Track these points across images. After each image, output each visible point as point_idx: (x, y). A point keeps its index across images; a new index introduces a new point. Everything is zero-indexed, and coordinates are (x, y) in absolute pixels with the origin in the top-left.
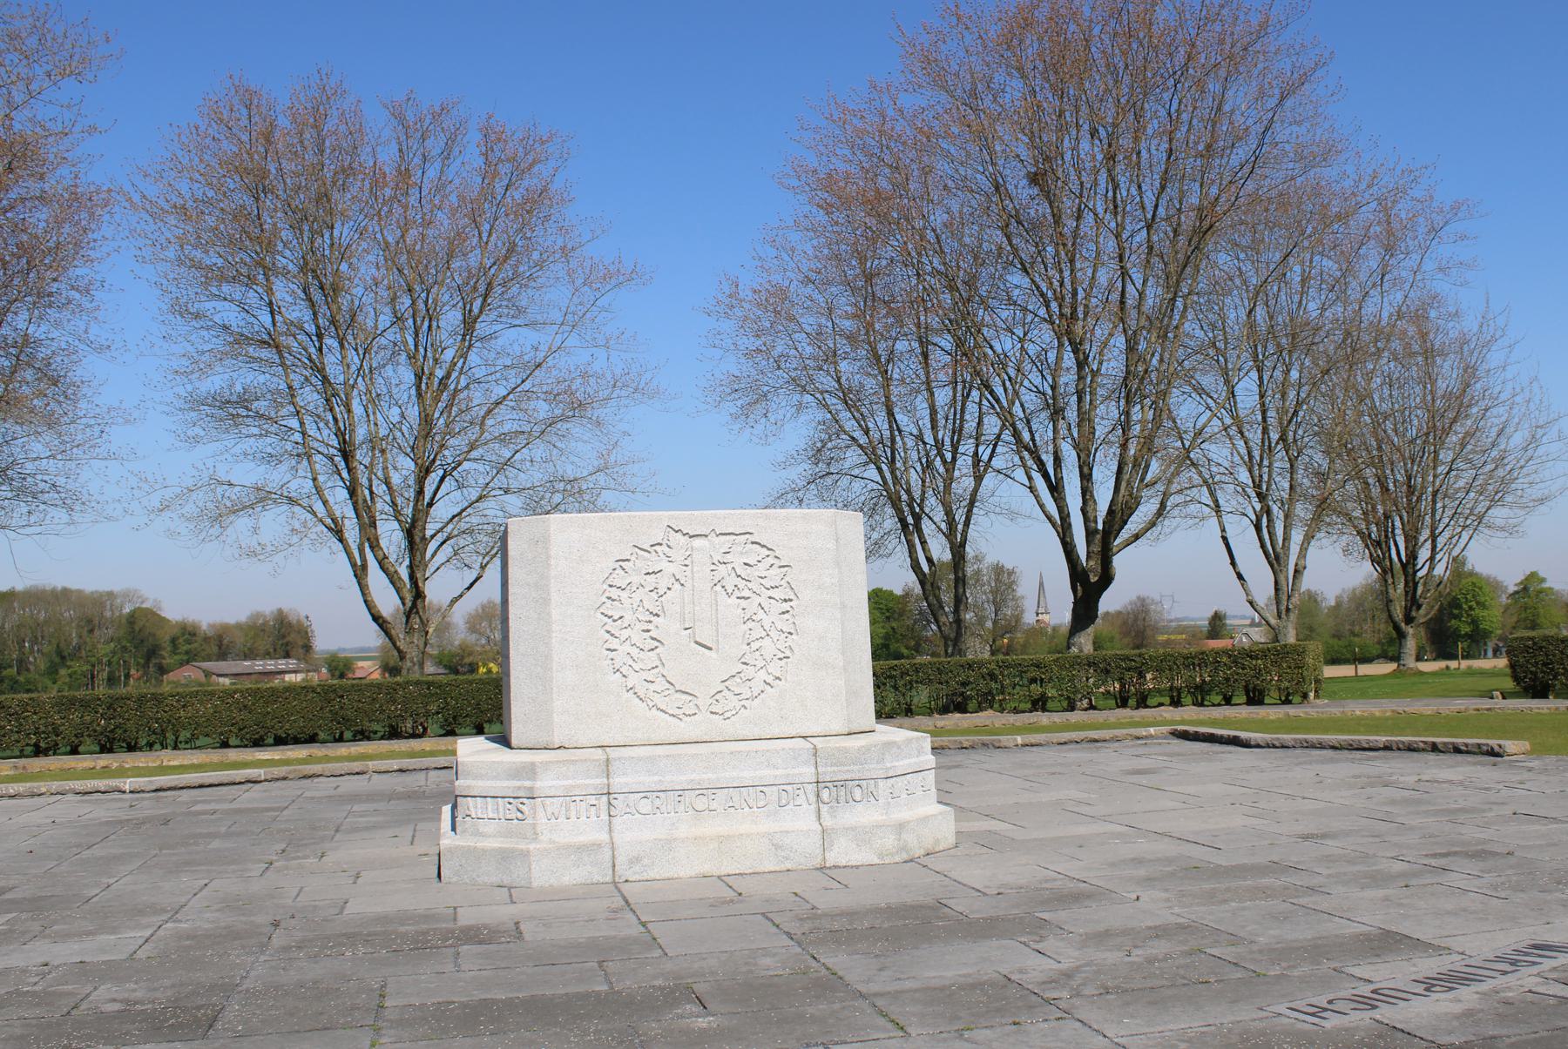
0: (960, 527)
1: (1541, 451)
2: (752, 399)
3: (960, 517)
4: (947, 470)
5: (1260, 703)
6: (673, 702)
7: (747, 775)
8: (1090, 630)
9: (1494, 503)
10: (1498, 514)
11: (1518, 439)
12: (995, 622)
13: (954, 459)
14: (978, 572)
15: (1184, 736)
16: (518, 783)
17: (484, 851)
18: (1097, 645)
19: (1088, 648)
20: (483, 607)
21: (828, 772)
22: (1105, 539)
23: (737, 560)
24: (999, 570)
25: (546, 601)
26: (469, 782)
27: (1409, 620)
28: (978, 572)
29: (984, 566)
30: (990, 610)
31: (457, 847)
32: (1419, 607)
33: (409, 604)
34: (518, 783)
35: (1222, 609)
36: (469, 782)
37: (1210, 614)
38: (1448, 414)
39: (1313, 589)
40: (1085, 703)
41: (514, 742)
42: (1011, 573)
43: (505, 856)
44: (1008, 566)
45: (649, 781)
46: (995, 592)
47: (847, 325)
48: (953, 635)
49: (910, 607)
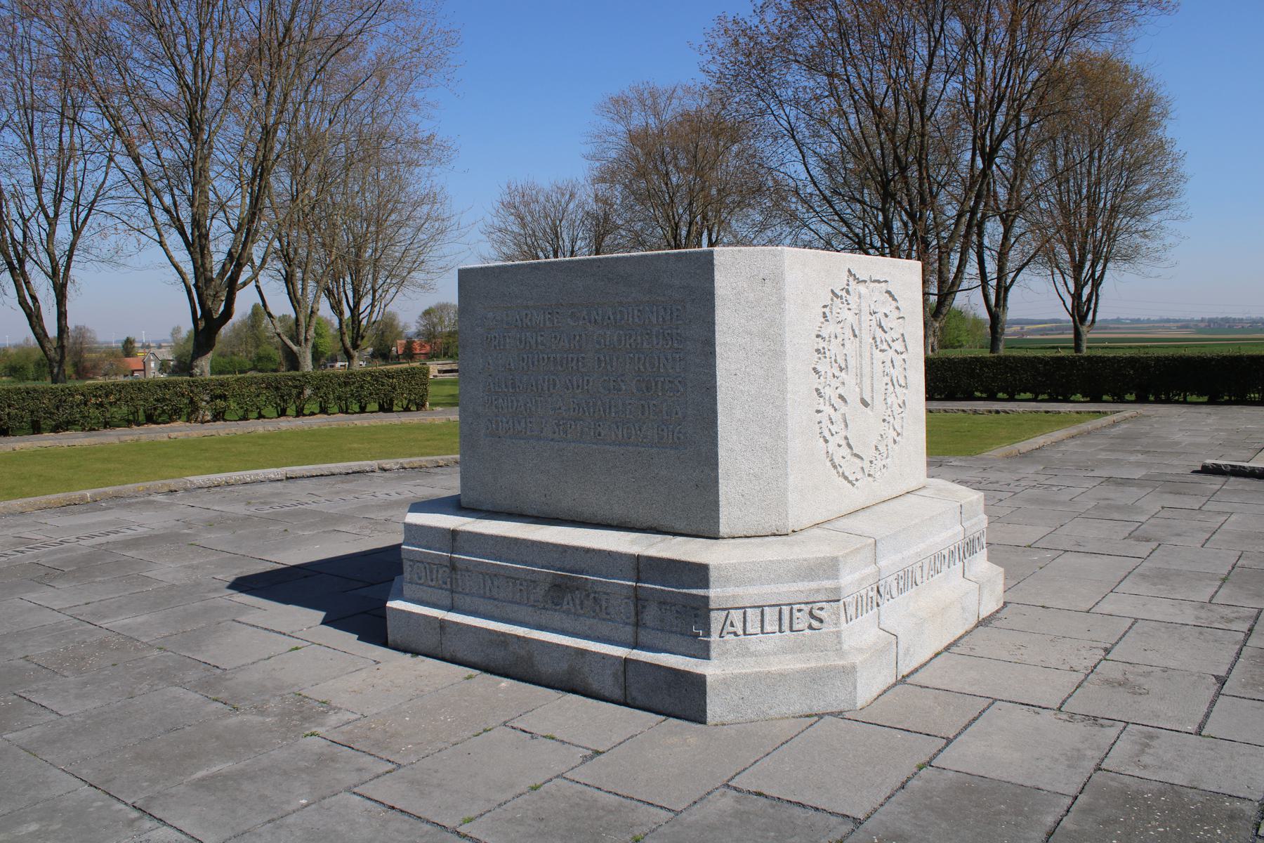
0: (62, 270)
4: (50, 224)
5: (390, 410)
8: (210, 355)
10: (418, 276)
13: (56, 215)
15: (1215, 471)
16: (814, 585)
17: (783, 676)
22: (1003, 290)
26: (730, 591)
27: (355, 346)
31: (736, 677)
32: (363, 338)
34: (814, 585)
35: (132, 336)
36: (730, 591)
39: (80, 324)
40: (256, 415)
41: (723, 529)
43: (814, 678)
47: (149, 84)
48: (58, 358)
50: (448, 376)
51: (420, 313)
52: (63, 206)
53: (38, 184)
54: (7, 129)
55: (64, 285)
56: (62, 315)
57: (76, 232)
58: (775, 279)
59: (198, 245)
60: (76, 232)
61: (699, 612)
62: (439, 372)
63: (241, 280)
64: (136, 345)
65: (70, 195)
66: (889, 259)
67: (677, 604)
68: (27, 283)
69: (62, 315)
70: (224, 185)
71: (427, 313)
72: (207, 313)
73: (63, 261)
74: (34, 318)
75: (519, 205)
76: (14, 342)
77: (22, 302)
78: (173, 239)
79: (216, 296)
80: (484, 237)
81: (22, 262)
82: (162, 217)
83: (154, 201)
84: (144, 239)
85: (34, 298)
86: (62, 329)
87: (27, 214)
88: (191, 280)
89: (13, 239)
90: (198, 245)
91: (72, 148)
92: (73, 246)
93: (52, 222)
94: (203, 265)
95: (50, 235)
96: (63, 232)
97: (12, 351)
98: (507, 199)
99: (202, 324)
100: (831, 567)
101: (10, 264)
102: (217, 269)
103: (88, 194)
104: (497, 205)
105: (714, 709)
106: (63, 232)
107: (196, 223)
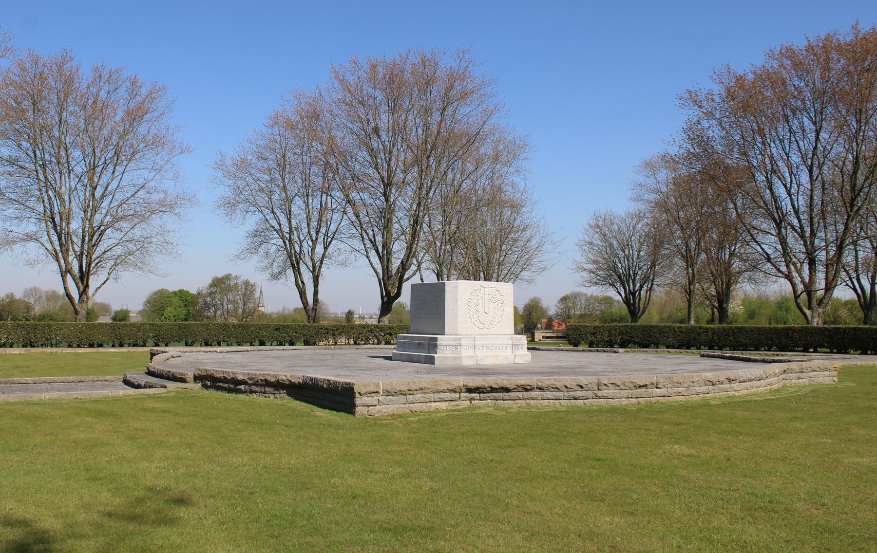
1: (544, 247)
2: (230, 206)
3: (318, 264)
6: (480, 325)
7: (500, 342)
8: (388, 316)
9: (523, 269)
10: (525, 274)
11: (533, 243)
12: (243, 310)
13: (317, 239)
14: (236, 284)
18: (390, 322)
19: (387, 323)
20: (31, 290)
21: (515, 342)
23: (493, 294)
24: (247, 284)
25: (457, 301)
28: (236, 284)
29: (239, 281)
30: (241, 303)
33: (82, 290)
35: (352, 309)
37: (347, 311)
38: (506, 232)
42: (253, 286)
43: (454, 358)
44: (252, 282)
45: (482, 343)
46: (245, 295)
49: (200, 300)
50: (548, 340)
51: (558, 299)
52: (320, 234)
53: (309, 219)
54: (297, 197)
55: (318, 277)
56: (316, 293)
57: (326, 248)
58: (457, 287)
59: (385, 257)
60: (326, 248)
61: (436, 346)
62: (543, 337)
63: (406, 277)
64: (355, 316)
65: (323, 230)
66: (482, 282)
67: (433, 346)
68: (300, 274)
69: (316, 293)
70: (401, 221)
71: (564, 299)
72: (388, 293)
73: (318, 264)
74: (302, 294)
75: (602, 227)
76: (276, 311)
77: (297, 285)
78: (373, 254)
79: (393, 284)
80: (577, 248)
81: (298, 263)
82: (369, 245)
83: (364, 234)
84: (358, 255)
85: (302, 282)
86: (316, 300)
87: (302, 238)
88: (381, 277)
89: (295, 251)
90: (385, 257)
91: (326, 208)
92: (324, 256)
93: (314, 243)
94: (387, 267)
95: (313, 250)
96: (319, 249)
97: (274, 316)
98: (593, 223)
99: (386, 299)
100: (460, 339)
101: (293, 265)
102: (394, 271)
103: (333, 227)
104: (587, 227)
105: (436, 362)
106: (319, 249)
107: (384, 246)
